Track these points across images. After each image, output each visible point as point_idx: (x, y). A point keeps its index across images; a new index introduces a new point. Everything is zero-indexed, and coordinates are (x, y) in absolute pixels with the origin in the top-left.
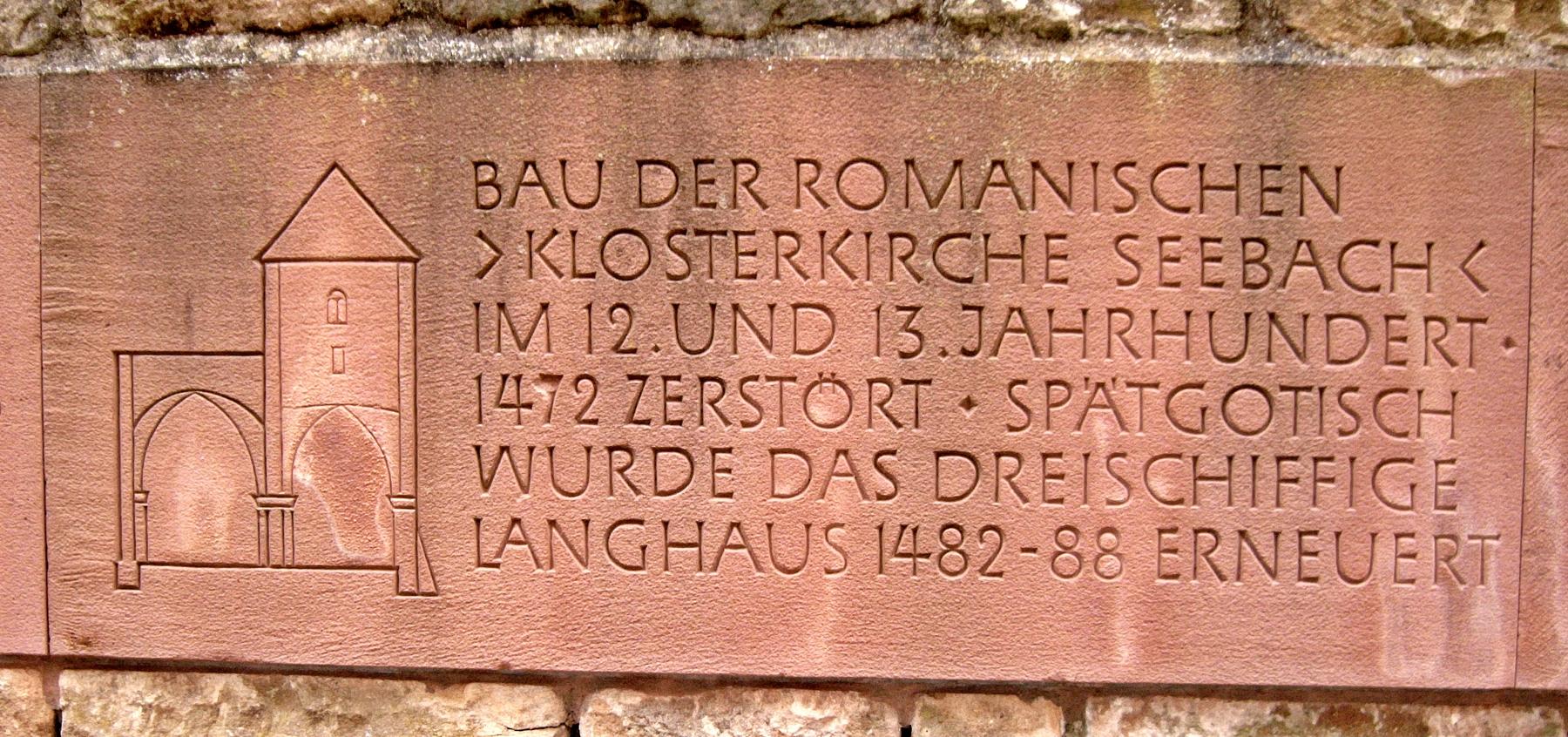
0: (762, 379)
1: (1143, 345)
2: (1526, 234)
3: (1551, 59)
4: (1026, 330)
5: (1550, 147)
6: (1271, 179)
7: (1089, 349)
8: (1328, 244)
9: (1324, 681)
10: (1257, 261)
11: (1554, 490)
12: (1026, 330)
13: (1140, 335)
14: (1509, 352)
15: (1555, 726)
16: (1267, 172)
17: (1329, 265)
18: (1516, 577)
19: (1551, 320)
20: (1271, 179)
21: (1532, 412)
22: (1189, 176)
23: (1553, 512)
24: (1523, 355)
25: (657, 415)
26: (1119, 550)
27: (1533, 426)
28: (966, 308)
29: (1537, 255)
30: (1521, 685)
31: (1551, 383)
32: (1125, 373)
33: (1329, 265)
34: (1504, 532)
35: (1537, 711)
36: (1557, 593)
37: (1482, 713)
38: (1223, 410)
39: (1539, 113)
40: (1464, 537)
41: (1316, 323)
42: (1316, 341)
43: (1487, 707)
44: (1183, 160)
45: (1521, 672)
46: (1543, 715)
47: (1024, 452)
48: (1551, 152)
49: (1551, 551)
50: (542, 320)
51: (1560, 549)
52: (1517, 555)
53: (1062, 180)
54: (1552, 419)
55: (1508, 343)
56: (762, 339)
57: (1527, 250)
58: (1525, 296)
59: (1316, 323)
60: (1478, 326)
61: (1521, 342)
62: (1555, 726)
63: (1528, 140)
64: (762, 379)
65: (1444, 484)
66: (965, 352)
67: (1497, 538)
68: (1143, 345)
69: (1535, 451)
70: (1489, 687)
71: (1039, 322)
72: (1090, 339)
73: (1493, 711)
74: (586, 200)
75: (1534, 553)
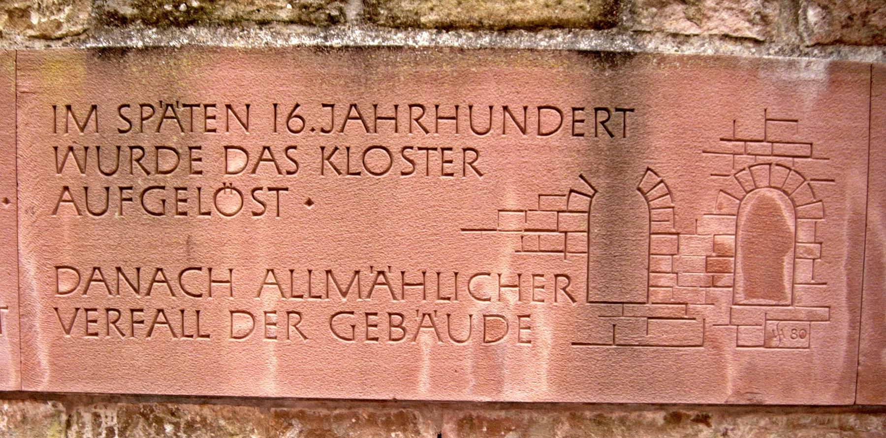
1: (431, 127)
2: (12, 141)
3: (27, 43)
4: (360, 118)
5: (24, 92)
11: (34, 282)
12: (360, 118)
13: (428, 120)
14: (6, 206)
15: (60, 412)
18: (17, 330)
19: (28, 188)
21: (20, 238)
23: (35, 294)
24: (14, 208)
27: (21, 246)
28: (324, 105)
29: (19, 152)
30: (24, 389)
31: (29, 222)
32: (417, 143)
34: (9, 305)
35: (50, 403)
36: (40, 337)
37: (21, 404)
38: (107, 207)
39: (19, 73)
41: (533, 110)
42: (533, 119)
43: (23, 400)
45: (24, 383)
46: (54, 406)
48: (24, 95)
49: (34, 316)
50: (93, 116)
51: (39, 314)
52: (17, 317)
54: (31, 242)
55: (6, 201)
56: (243, 125)
57: (14, 150)
58: (14, 175)
59: (533, 110)
61: (12, 200)
62: (60, 412)
63: (13, 89)
65: (538, 287)
66: (323, 131)
67: (6, 308)
68: (431, 127)
69: (23, 260)
70: (8, 390)
71: (369, 115)
73: (26, 403)
75: (26, 317)
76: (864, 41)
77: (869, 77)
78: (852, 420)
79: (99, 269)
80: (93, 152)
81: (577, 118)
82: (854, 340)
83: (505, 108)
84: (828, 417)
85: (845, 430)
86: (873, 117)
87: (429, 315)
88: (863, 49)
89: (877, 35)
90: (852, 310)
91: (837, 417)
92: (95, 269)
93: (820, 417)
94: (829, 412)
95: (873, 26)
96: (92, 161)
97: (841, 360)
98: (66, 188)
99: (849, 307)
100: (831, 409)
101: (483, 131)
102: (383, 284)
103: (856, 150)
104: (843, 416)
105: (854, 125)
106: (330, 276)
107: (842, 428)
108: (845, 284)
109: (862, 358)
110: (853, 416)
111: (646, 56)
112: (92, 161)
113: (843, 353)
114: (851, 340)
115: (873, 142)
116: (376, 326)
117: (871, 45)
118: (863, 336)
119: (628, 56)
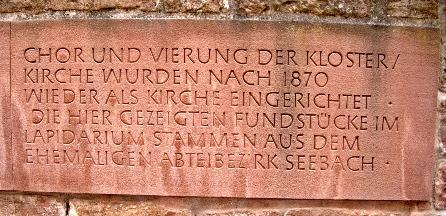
0: (187, 112)
6: (280, 54)
7: (245, 103)
8: (239, 72)
9: (356, 199)
10: (295, 78)
16: (278, 52)
17: (241, 79)
20: (280, 54)
22: (36, 52)
25: (155, 123)
26: (222, 160)
33: (241, 79)
40: (184, 154)
42: (125, 53)
44: (34, 47)
47: (101, 132)
53: (225, 54)
56: (257, 102)
60: (349, 97)
64: (187, 112)
65: (334, 142)
72: (340, 103)
74: (100, 60)
76: (8, 11)
77: (9, 28)
78: (21, 198)
79: (39, 131)
80: (123, 72)
81: (368, 59)
82: (9, 159)
83: (217, 50)
84: (7, 196)
85: (17, 203)
86: (11, 49)
87: (339, 157)
88: (9, 14)
89: (14, 7)
90: (7, 144)
91: (12, 196)
92: (269, 135)
93: (3, 196)
94: (9, 194)
95: (12, 3)
96: (123, 77)
97: (4, 168)
98: (112, 91)
99: (6, 142)
100: (9, 192)
101: (204, 61)
102: (40, 137)
103: (4, 65)
104: (15, 196)
105: (2, 52)
106: (345, 139)
107: (16, 202)
108: (2, 131)
109: (14, 168)
110: (21, 196)
111: (393, 27)
112: (123, 77)
113: (5, 165)
114: (8, 158)
115: (12, 60)
116: (303, 162)
117: (13, 12)
118: (14, 157)
119: (387, 27)
